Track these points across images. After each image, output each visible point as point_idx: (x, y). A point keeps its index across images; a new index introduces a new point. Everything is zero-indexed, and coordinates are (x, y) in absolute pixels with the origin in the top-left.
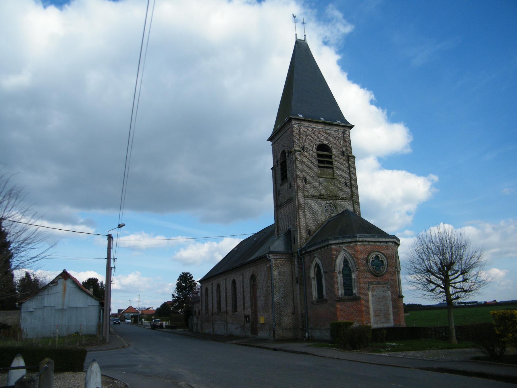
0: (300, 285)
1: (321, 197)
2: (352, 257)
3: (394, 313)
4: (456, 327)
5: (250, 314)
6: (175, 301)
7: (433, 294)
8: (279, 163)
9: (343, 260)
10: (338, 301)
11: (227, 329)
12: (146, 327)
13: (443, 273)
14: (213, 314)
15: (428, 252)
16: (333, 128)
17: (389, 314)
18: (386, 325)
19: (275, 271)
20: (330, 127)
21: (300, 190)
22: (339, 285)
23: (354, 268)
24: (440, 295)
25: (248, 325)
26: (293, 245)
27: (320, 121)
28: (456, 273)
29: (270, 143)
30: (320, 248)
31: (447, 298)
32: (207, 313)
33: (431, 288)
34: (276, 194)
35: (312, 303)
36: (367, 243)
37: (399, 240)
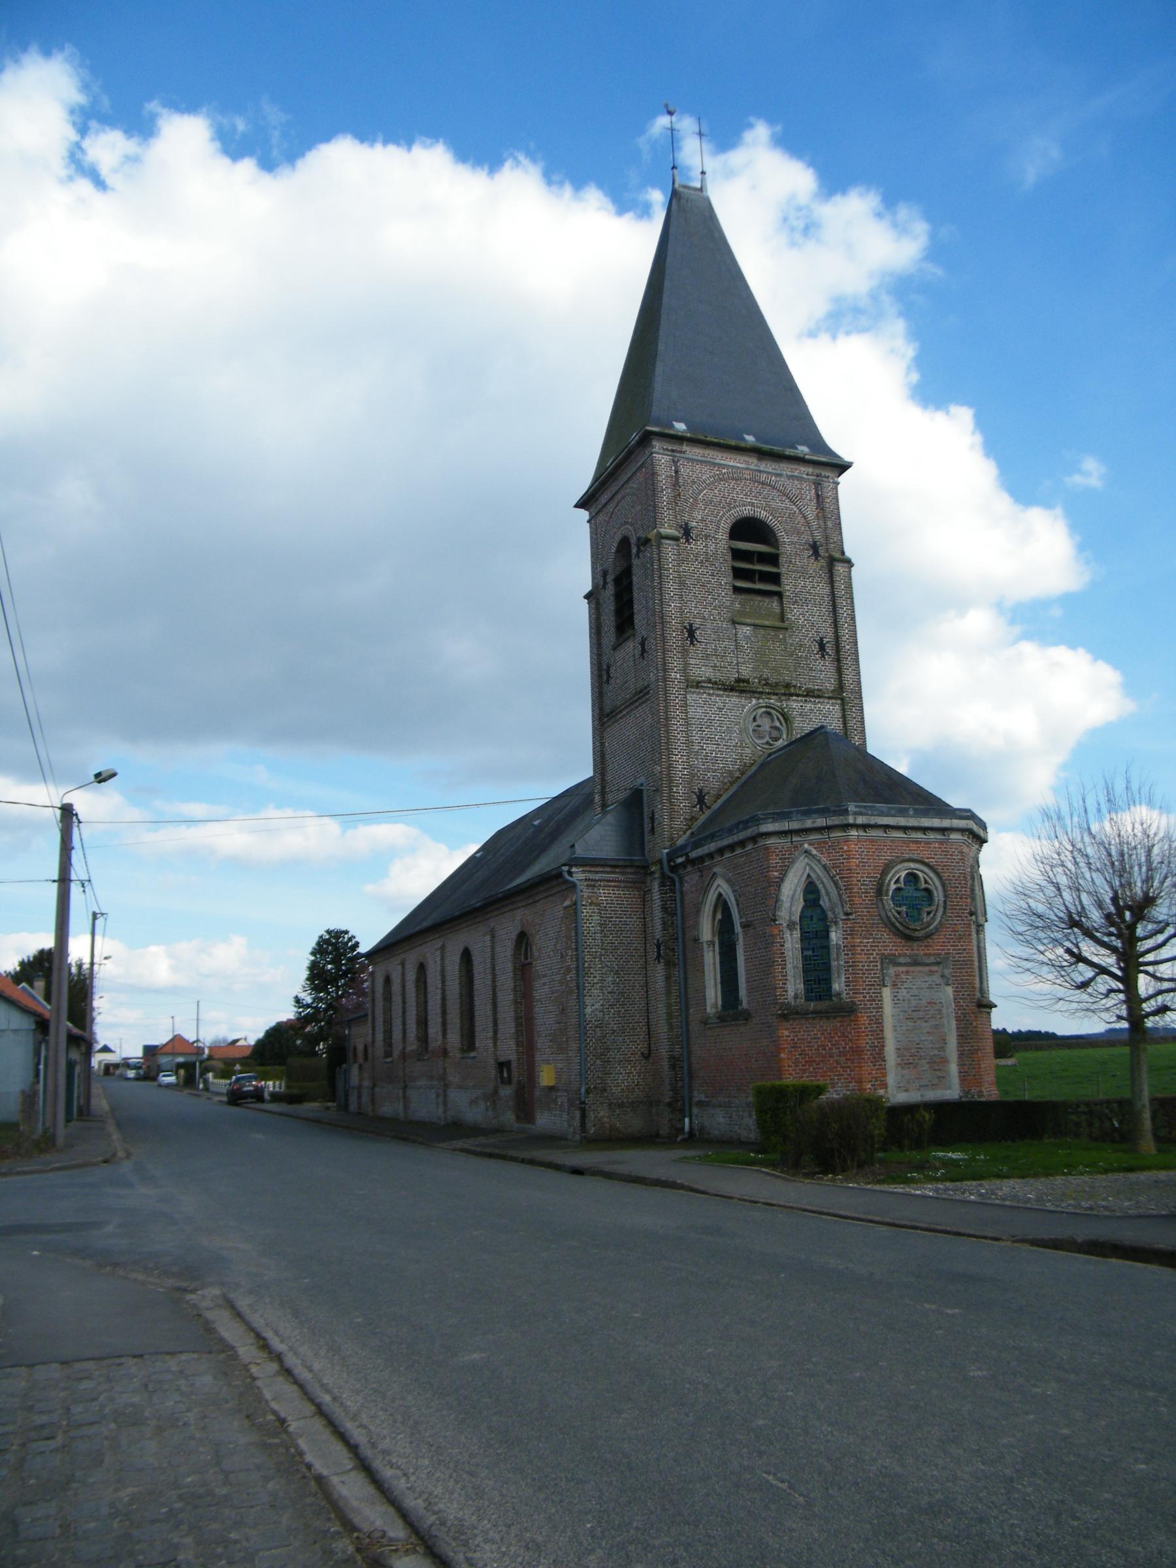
0: (669, 964)
1: (739, 687)
2: (832, 878)
3: (961, 1055)
4: (1153, 1100)
5: (513, 1057)
6: (302, 1021)
7: (1085, 997)
8: (610, 578)
9: (802, 886)
10: (784, 1017)
11: (445, 1103)
12: (217, 1098)
13: (1119, 929)
14: (404, 1056)
15: (1076, 863)
16: (786, 468)
17: (945, 1061)
18: (932, 1095)
19: (590, 918)
20: (775, 465)
21: (675, 663)
22: (789, 966)
23: (839, 910)
24: (1109, 1002)
25: (506, 1092)
26: (647, 837)
27: (743, 445)
28: (1161, 931)
29: (584, 514)
30: (731, 848)
31: (1130, 1009)
32: (388, 1054)
33: (1080, 979)
34: (600, 676)
35: (705, 1022)
36: (880, 833)
37: (984, 827)
